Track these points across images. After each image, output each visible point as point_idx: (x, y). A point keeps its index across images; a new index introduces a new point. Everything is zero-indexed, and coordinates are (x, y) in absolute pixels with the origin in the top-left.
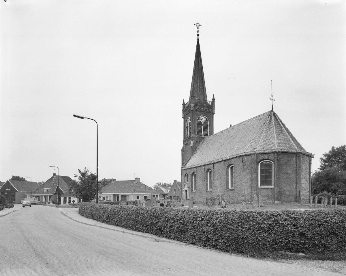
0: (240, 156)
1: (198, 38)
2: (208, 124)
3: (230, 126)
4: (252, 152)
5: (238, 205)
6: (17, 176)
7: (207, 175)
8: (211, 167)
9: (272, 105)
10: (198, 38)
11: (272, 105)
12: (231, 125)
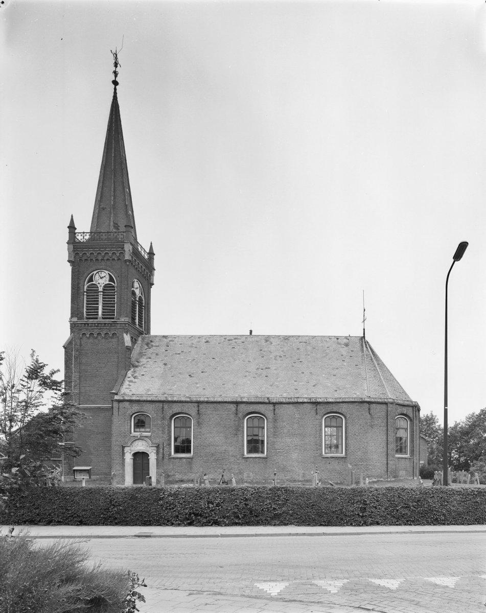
0: (363, 402)
1: (115, 89)
2: (85, 296)
3: (249, 334)
4: (390, 400)
5: (191, 483)
6: (421, 408)
7: (171, 422)
8: (267, 410)
9: (364, 329)
10: (115, 89)
11: (364, 329)
12: (251, 331)
